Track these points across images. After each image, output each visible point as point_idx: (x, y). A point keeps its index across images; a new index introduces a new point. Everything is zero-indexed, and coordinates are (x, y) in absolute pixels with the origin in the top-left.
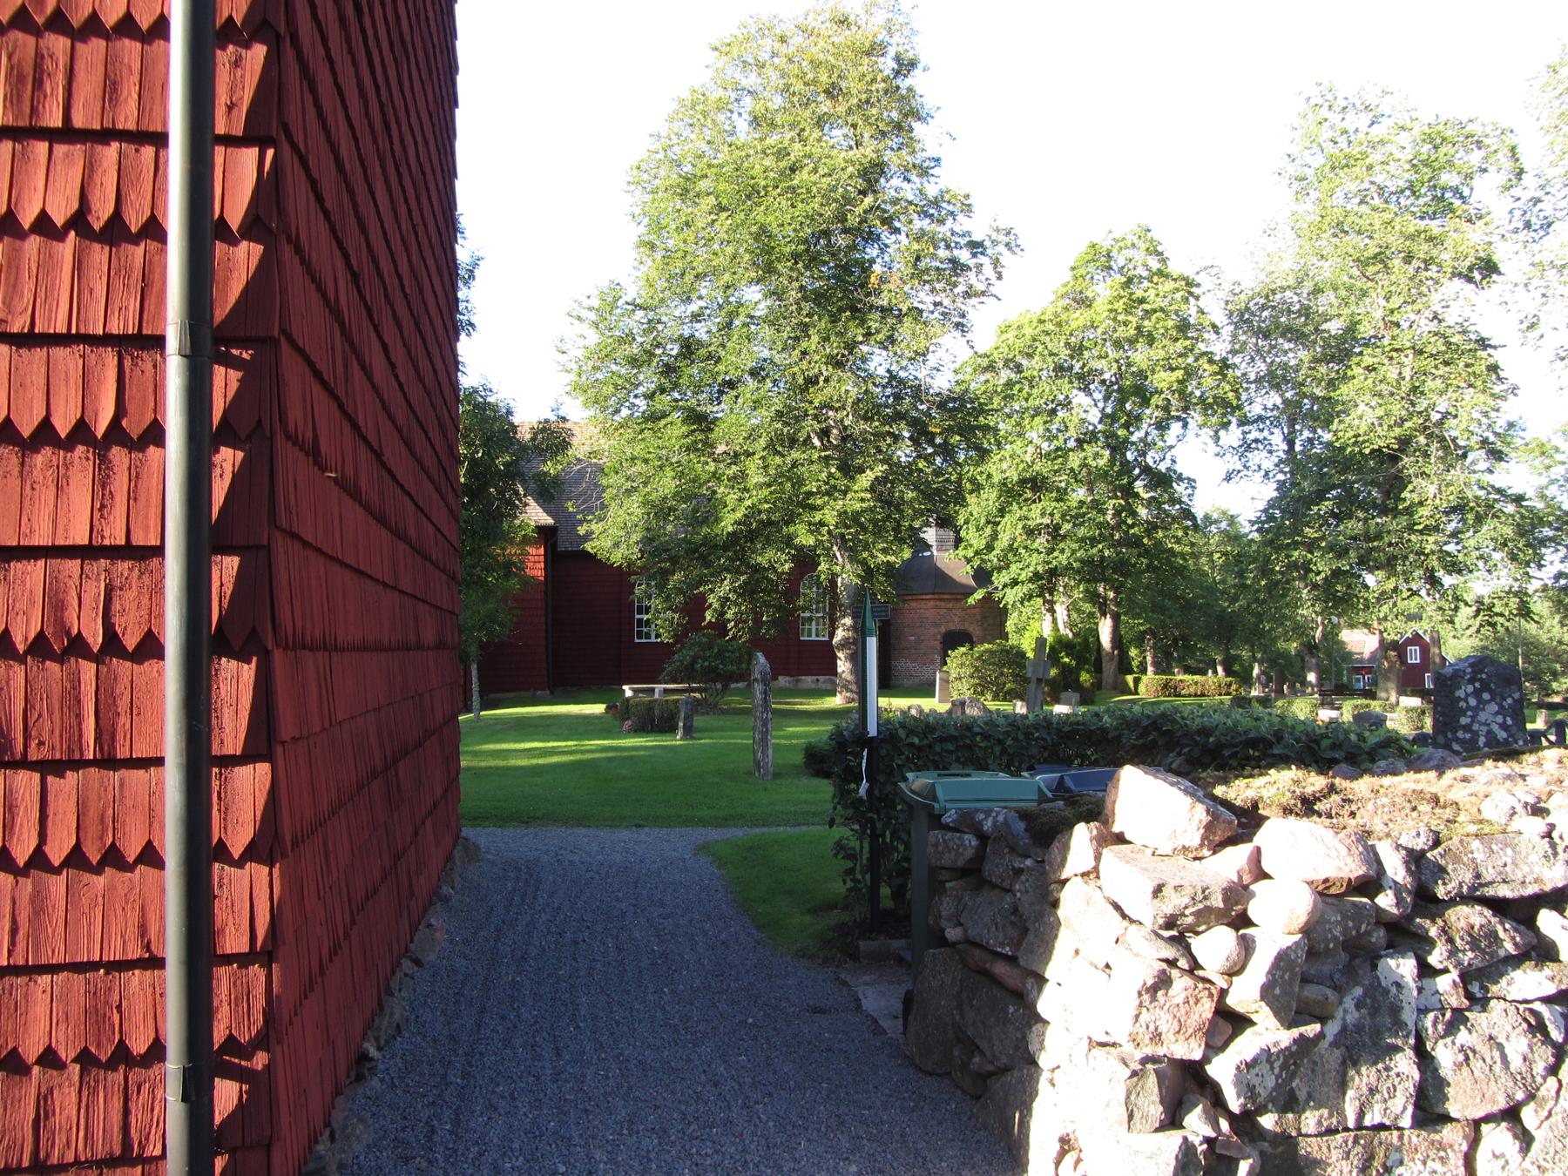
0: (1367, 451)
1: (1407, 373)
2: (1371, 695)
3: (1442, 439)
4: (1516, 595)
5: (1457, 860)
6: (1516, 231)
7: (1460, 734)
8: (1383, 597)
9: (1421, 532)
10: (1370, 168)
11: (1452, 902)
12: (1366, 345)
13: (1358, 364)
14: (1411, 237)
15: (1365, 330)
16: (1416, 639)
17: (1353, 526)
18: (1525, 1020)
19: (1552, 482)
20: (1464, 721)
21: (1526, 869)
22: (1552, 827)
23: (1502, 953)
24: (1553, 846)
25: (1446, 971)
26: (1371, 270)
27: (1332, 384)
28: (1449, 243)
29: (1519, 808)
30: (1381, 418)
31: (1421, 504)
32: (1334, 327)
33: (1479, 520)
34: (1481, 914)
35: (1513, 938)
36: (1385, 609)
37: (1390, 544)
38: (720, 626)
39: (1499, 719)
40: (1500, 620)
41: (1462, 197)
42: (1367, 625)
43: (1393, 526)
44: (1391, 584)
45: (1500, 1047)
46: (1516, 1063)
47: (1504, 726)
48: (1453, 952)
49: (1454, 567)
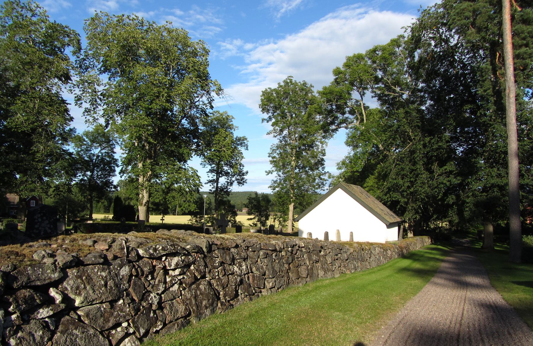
0: (20, 131)
1: (37, 106)
2: (15, 217)
3: (47, 131)
4: (67, 185)
5: (22, 274)
6: (77, 67)
7: (35, 231)
8: (22, 183)
9: (37, 162)
10: (30, 31)
11: (19, 289)
12: (23, 93)
13: (19, 100)
14: (42, 59)
15: (23, 88)
16: (34, 198)
17: (12, 156)
18: (42, 325)
19: (82, 150)
20: (36, 226)
21: (46, 275)
22: (56, 261)
23: (35, 304)
24: (56, 267)
25: (15, 313)
26: (27, 67)
27: (9, 105)
28: (55, 66)
29: (46, 255)
30: (25, 120)
31: (38, 152)
32: (12, 84)
33: (57, 160)
34: (29, 292)
35: (40, 299)
36: (22, 187)
37: (26, 165)
38: (105, 188)
39: (49, 226)
40: (62, 193)
41: (61, 51)
42: (16, 192)
43: (27, 158)
44: (25, 179)
45: (33, 335)
46: (38, 338)
47: (50, 228)
48: (18, 306)
49: (48, 175)
